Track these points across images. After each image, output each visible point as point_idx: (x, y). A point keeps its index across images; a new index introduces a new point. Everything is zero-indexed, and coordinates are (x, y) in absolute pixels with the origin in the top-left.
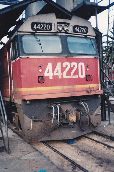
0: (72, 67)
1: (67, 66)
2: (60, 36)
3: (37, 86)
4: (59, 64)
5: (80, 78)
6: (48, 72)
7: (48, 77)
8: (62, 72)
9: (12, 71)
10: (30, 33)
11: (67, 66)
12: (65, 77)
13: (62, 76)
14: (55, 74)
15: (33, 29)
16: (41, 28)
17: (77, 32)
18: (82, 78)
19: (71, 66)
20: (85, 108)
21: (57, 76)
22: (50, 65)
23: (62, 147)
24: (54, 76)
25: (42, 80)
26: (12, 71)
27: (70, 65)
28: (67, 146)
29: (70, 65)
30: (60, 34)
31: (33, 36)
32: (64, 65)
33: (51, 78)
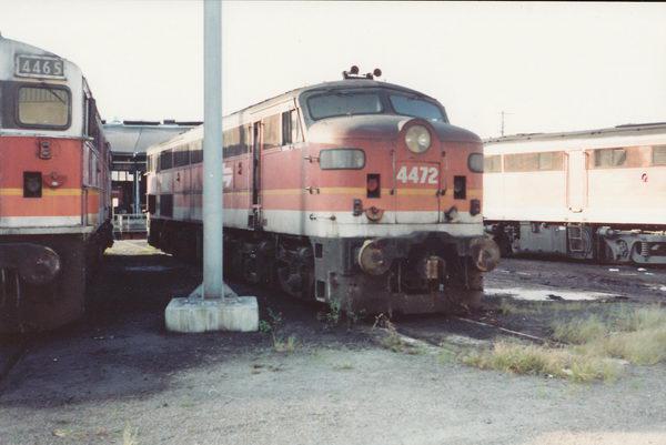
14: (410, 178)
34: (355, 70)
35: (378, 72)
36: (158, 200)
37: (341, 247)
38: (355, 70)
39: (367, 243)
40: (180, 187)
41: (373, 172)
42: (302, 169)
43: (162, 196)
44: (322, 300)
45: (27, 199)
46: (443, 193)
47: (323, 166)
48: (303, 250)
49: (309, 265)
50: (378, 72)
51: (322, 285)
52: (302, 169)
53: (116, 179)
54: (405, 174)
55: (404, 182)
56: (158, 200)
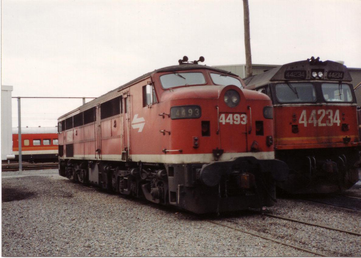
1: (322, 113)
2: (312, 83)
3: (290, 136)
4: (314, 112)
5: (332, 110)
6: (303, 120)
7: (303, 124)
8: (317, 119)
9: (310, 162)
10: (283, 82)
11: (322, 113)
12: (320, 125)
13: (317, 124)
15: (285, 77)
16: (320, 120)
17: (331, 78)
19: (327, 114)
20: (300, 81)
22: (304, 113)
23: (172, 232)
25: (296, 129)
26: (310, 162)
27: (326, 113)
28: (189, 223)
29: (326, 113)
30: (312, 81)
31: (287, 84)
33: (305, 125)
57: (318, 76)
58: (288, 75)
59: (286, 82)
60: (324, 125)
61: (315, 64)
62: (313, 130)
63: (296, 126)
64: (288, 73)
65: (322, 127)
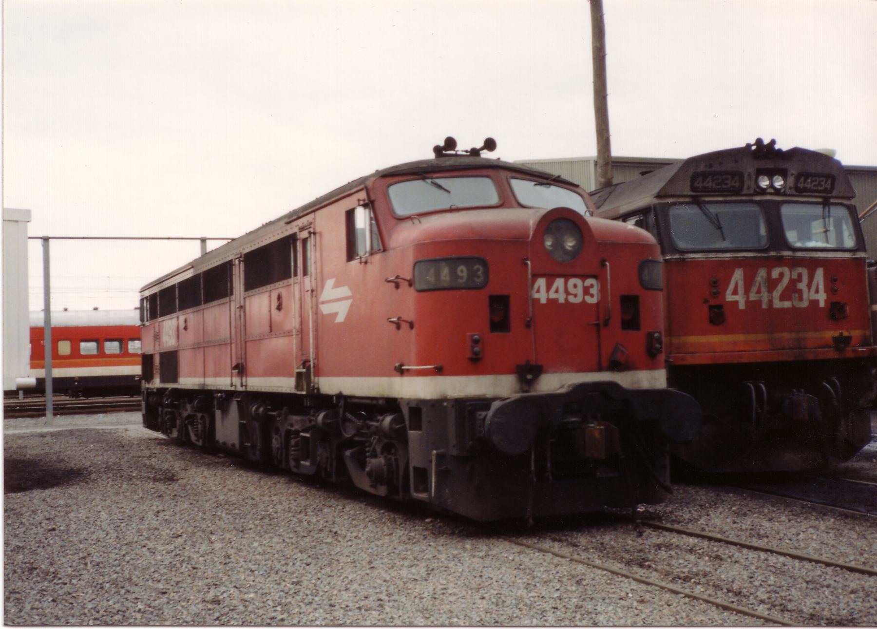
0: (775, 279)
1: (781, 275)
2: (758, 203)
3: (704, 333)
4: (762, 273)
6: (735, 292)
10: (687, 200)
11: (781, 275)
12: (778, 304)
13: (771, 302)
14: (552, 295)
15: (693, 189)
17: (805, 190)
18: (592, 305)
19: (793, 277)
21: (817, 301)
22: (738, 275)
24: (548, 300)
25: (718, 316)
32: (775, 273)
33: (742, 306)
34: (450, 143)
35: (490, 144)
36: (157, 360)
37: (452, 418)
38: (450, 143)
39: (496, 405)
40: (189, 338)
41: (500, 291)
42: (420, 291)
43: (163, 355)
44: (423, 496)
45: (505, 293)
46: (606, 323)
47: (419, 287)
48: (388, 419)
49: (396, 440)
50: (490, 144)
51: (422, 474)
52: (420, 291)
53: (137, 342)
54: (543, 289)
55: (543, 301)
56: (157, 360)
57: (771, 186)
58: (699, 184)
59: (696, 201)
60: (787, 304)
61: (764, 156)
62: (760, 317)
63: (720, 307)
64: (700, 179)
65: (783, 310)
